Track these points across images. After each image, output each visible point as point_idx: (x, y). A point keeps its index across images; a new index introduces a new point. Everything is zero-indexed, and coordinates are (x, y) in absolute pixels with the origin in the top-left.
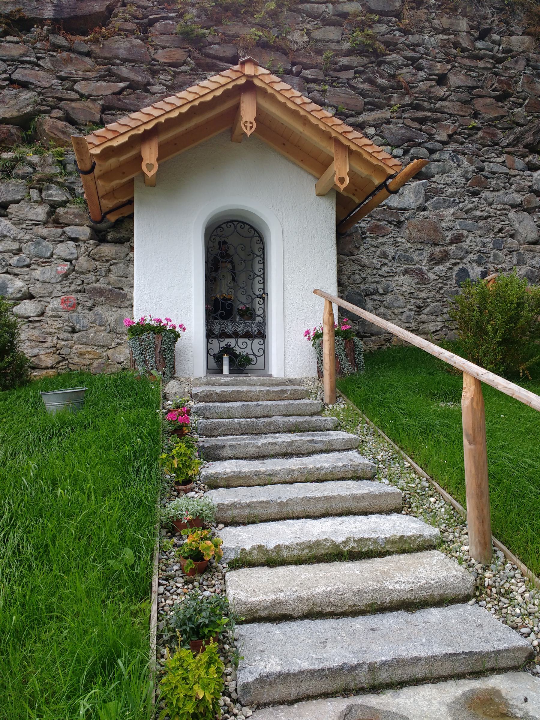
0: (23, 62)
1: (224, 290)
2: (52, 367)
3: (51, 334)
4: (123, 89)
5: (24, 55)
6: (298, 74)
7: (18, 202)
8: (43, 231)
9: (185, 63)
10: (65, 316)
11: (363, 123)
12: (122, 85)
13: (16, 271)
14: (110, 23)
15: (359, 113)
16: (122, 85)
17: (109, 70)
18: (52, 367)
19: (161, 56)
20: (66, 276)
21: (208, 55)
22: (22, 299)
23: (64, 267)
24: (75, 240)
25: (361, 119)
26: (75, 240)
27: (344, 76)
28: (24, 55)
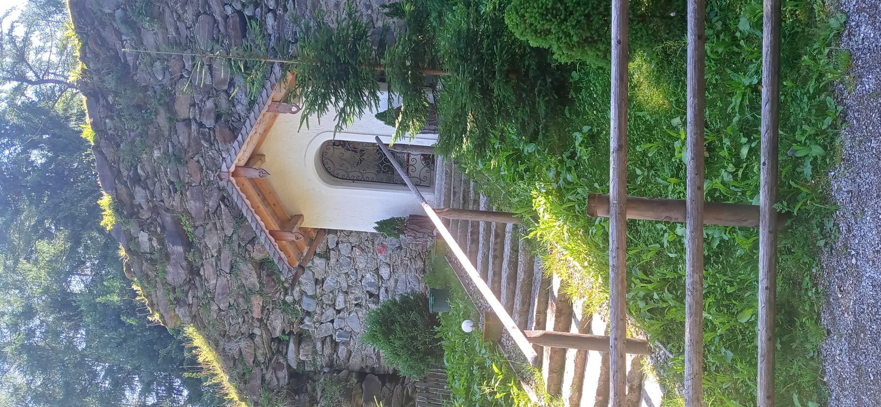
0: (217, 265)
1: (621, 323)
2: (424, 262)
3: (402, 261)
4: (226, 205)
5: (212, 265)
6: (189, 73)
7: (313, 273)
8: (333, 261)
9: (198, 161)
10: (390, 252)
11: (223, 18)
12: (222, 206)
13: (360, 277)
14: (23, 306)
15: (215, 21)
16: (222, 206)
17: (214, 214)
18: (424, 262)
19: (197, 178)
20: (363, 250)
21: (189, 145)
22: (378, 275)
23: (357, 252)
24: (337, 244)
25: (219, 19)
26: (337, 244)
27: (184, 32)
28: (212, 265)
